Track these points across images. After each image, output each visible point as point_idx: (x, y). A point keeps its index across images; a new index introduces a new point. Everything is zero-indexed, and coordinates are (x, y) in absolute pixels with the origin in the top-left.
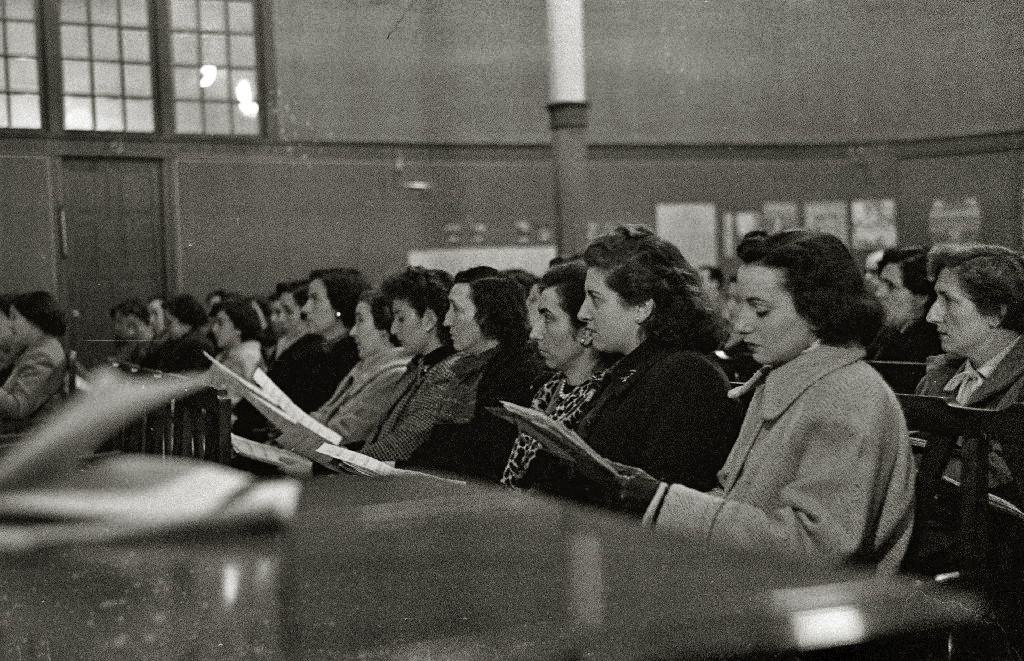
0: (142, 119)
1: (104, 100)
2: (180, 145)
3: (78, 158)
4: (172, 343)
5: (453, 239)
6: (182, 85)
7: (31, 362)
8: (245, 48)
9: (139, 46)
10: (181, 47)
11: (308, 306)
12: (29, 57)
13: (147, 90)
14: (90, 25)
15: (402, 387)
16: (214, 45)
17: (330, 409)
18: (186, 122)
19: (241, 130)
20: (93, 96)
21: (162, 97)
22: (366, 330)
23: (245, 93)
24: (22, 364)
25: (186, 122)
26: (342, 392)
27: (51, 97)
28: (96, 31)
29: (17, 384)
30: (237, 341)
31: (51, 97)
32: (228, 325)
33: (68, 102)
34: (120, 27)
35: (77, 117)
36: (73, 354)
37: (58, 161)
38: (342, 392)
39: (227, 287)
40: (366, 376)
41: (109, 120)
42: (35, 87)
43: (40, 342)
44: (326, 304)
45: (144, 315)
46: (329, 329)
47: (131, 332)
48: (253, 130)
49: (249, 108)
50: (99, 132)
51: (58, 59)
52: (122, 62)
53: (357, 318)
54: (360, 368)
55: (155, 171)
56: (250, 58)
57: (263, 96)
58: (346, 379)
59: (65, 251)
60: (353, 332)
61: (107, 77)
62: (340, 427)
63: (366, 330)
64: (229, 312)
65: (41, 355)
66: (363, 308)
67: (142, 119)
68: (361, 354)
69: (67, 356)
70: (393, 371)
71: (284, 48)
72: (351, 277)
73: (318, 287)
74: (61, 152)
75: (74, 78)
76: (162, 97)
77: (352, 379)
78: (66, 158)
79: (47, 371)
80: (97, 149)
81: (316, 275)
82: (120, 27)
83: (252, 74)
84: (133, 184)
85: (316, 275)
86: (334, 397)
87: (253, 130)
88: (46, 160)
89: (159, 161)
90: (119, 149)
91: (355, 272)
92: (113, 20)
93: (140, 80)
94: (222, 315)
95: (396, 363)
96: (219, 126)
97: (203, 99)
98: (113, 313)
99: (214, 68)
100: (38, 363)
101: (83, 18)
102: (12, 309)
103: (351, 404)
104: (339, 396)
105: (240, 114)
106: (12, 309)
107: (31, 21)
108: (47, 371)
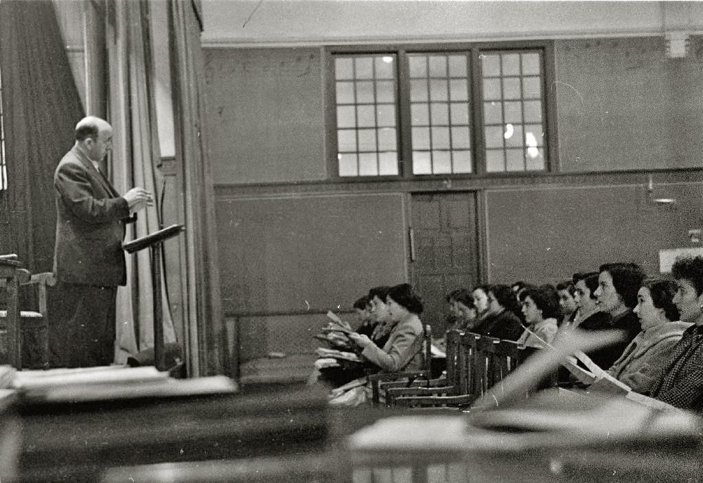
0: (463, 165)
1: (437, 152)
2: (489, 181)
3: (422, 193)
4: (492, 318)
5: (694, 240)
6: (491, 138)
7: (401, 332)
8: (535, 110)
9: (462, 114)
10: (490, 112)
11: (598, 292)
12: (390, 127)
13: (340, 110)
14: (429, 103)
15: (679, 350)
16: (513, 109)
17: (618, 368)
18: (493, 164)
19: (530, 168)
20: (431, 150)
21: (477, 150)
22: (647, 309)
23: (533, 141)
24: (396, 333)
25: (493, 164)
26: (629, 353)
27: (404, 152)
28: (434, 106)
29: (392, 347)
30: (540, 317)
31: (404, 152)
32: (533, 307)
33: (415, 156)
34: (449, 102)
35: (421, 166)
36: (428, 327)
37: (410, 195)
38: (629, 353)
39: (527, 281)
40: (647, 343)
41: (442, 168)
42: (395, 147)
43: (408, 318)
44: (611, 289)
45: (469, 302)
46: (615, 308)
47: (461, 313)
48: (540, 166)
49: (534, 152)
50: (436, 175)
51: (410, 127)
52: (450, 126)
53: (639, 299)
54: (643, 336)
55: (472, 200)
56: (539, 117)
57: (548, 145)
58: (630, 345)
59: (413, 258)
60: (636, 310)
61: (441, 137)
62: (631, 382)
63: (647, 309)
64: (533, 297)
65: (407, 327)
66: (644, 292)
67: (463, 165)
68: (643, 327)
69: (425, 328)
70: (670, 339)
71: (563, 108)
72: (632, 269)
73: (606, 277)
74: (410, 190)
75: (419, 139)
76: (477, 150)
77: (635, 345)
78: (413, 194)
79: (412, 338)
80: (434, 187)
81: (603, 268)
82: (449, 102)
83: (540, 128)
84: (459, 209)
85: (603, 268)
86: (622, 357)
87: (540, 166)
88: (401, 196)
89: (475, 192)
90: (449, 185)
91: (634, 266)
92: (445, 98)
93: (463, 138)
94: (528, 299)
95: (672, 333)
96: (516, 166)
97: (505, 147)
98: (448, 299)
99: (203, 33)
100: (406, 333)
101: (425, 98)
102: (388, 298)
103: (635, 364)
104: (625, 357)
105: (530, 157)
106: (388, 298)
107: (467, 126)
108: (412, 338)
